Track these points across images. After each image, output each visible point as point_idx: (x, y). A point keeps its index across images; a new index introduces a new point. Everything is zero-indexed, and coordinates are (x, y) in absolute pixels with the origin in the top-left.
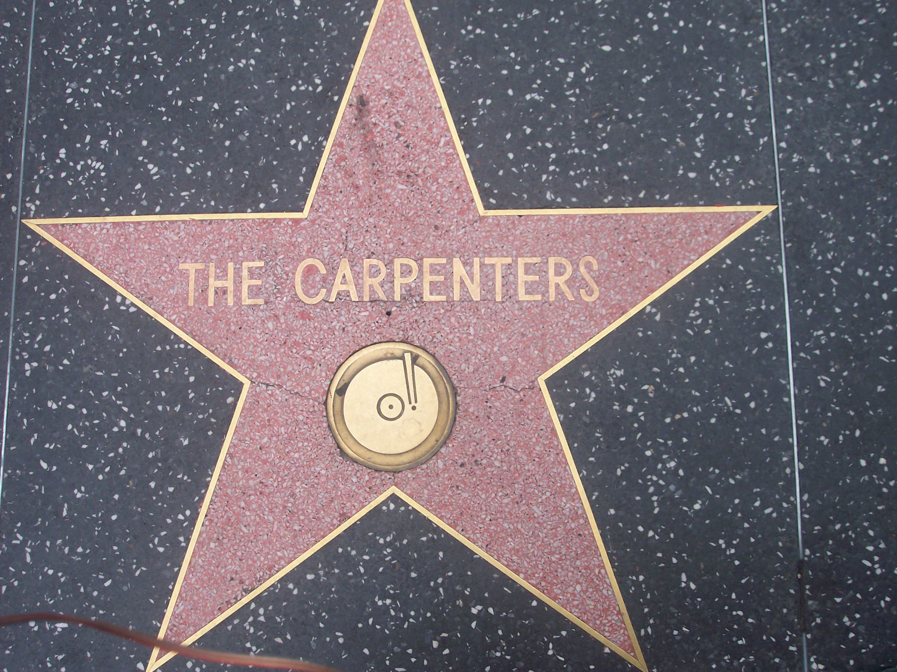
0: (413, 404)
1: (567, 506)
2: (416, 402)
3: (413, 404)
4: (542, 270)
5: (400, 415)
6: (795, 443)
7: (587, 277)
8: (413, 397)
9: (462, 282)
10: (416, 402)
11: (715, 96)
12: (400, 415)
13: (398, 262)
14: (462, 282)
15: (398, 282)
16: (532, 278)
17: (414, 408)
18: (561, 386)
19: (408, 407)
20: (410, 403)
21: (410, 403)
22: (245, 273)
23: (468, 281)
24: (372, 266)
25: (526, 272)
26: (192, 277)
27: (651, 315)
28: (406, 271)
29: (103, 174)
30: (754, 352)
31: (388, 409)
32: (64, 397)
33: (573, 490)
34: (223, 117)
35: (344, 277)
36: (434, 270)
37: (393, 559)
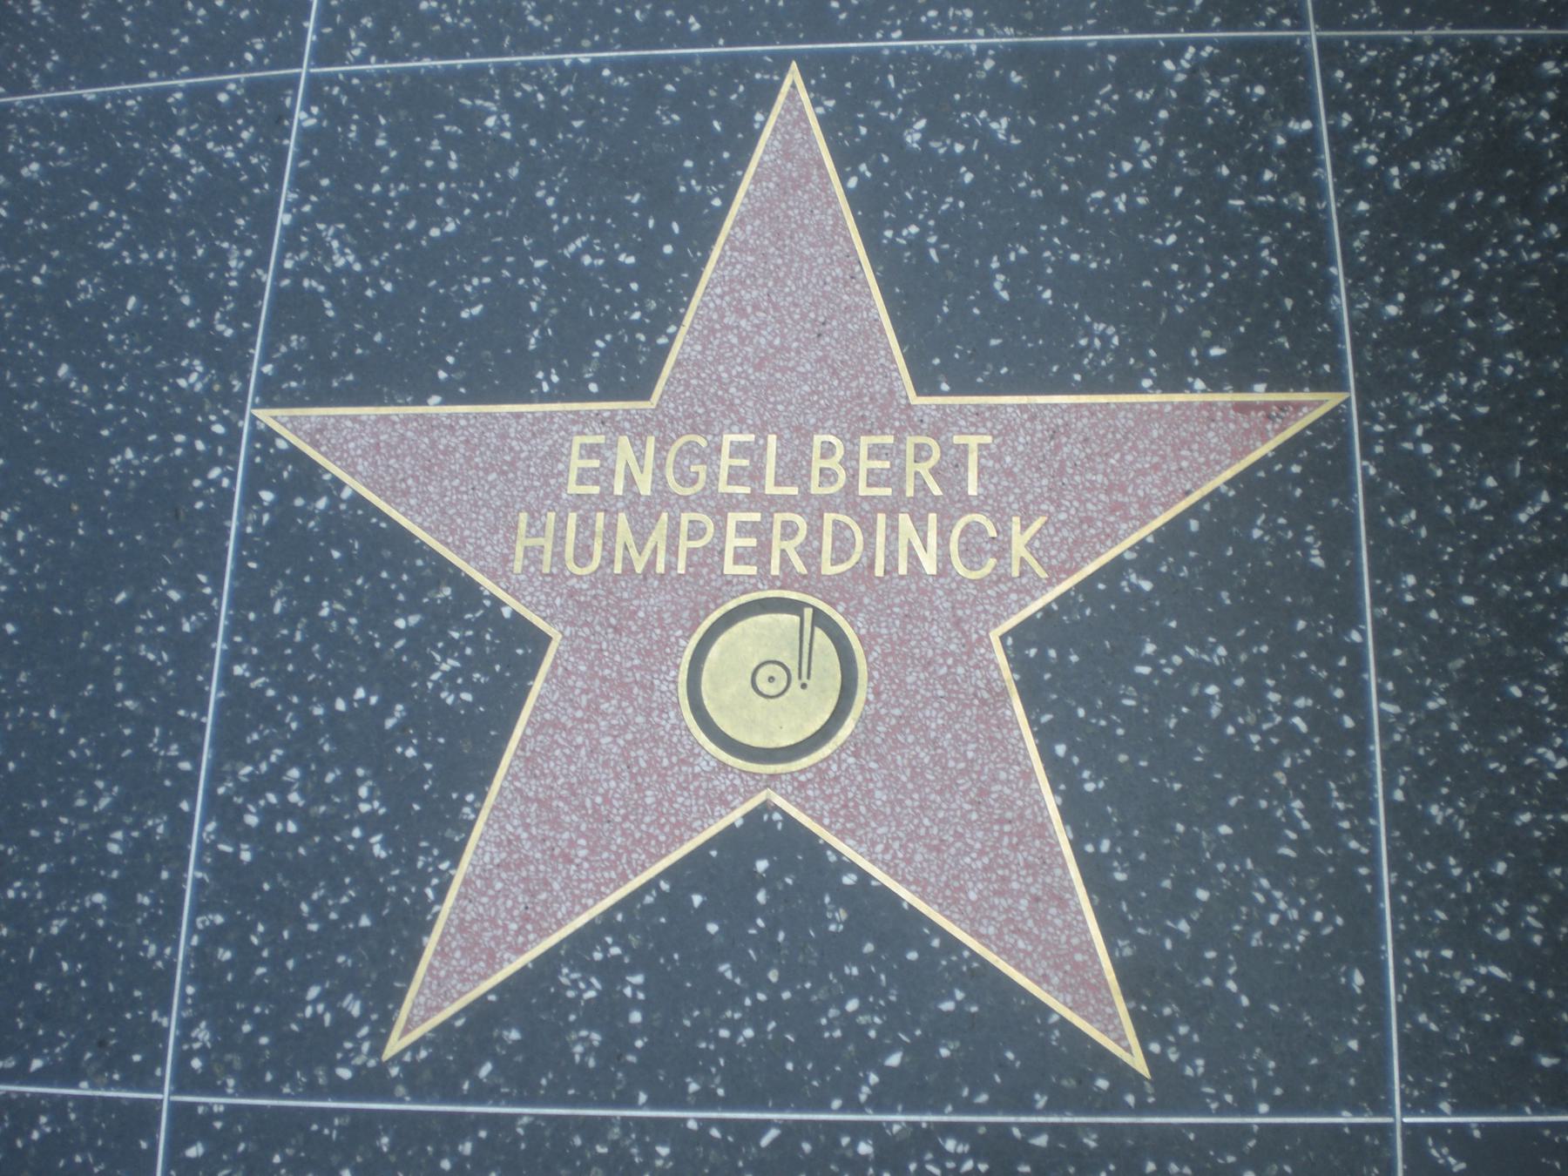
0: (804, 679)
1: (639, 856)
2: (809, 677)
3: (804, 679)
5: (785, 690)
6: (945, 1119)
8: (805, 653)
9: (911, 548)
10: (809, 677)
11: (1483, 404)
12: (785, 690)
14: (911, 548)
15: (684, 545)
16: (877, 464)
17: (804, 686)
19: (795, 683)
23: (917, 543)
24: (785, 524)
27: (281, 139)
28: (828, 451)
29: (450, 359)
30: (442, 116)
31: (765, 691)
33: (697, 824)
36: (875, 452)
37: (1522, 427)
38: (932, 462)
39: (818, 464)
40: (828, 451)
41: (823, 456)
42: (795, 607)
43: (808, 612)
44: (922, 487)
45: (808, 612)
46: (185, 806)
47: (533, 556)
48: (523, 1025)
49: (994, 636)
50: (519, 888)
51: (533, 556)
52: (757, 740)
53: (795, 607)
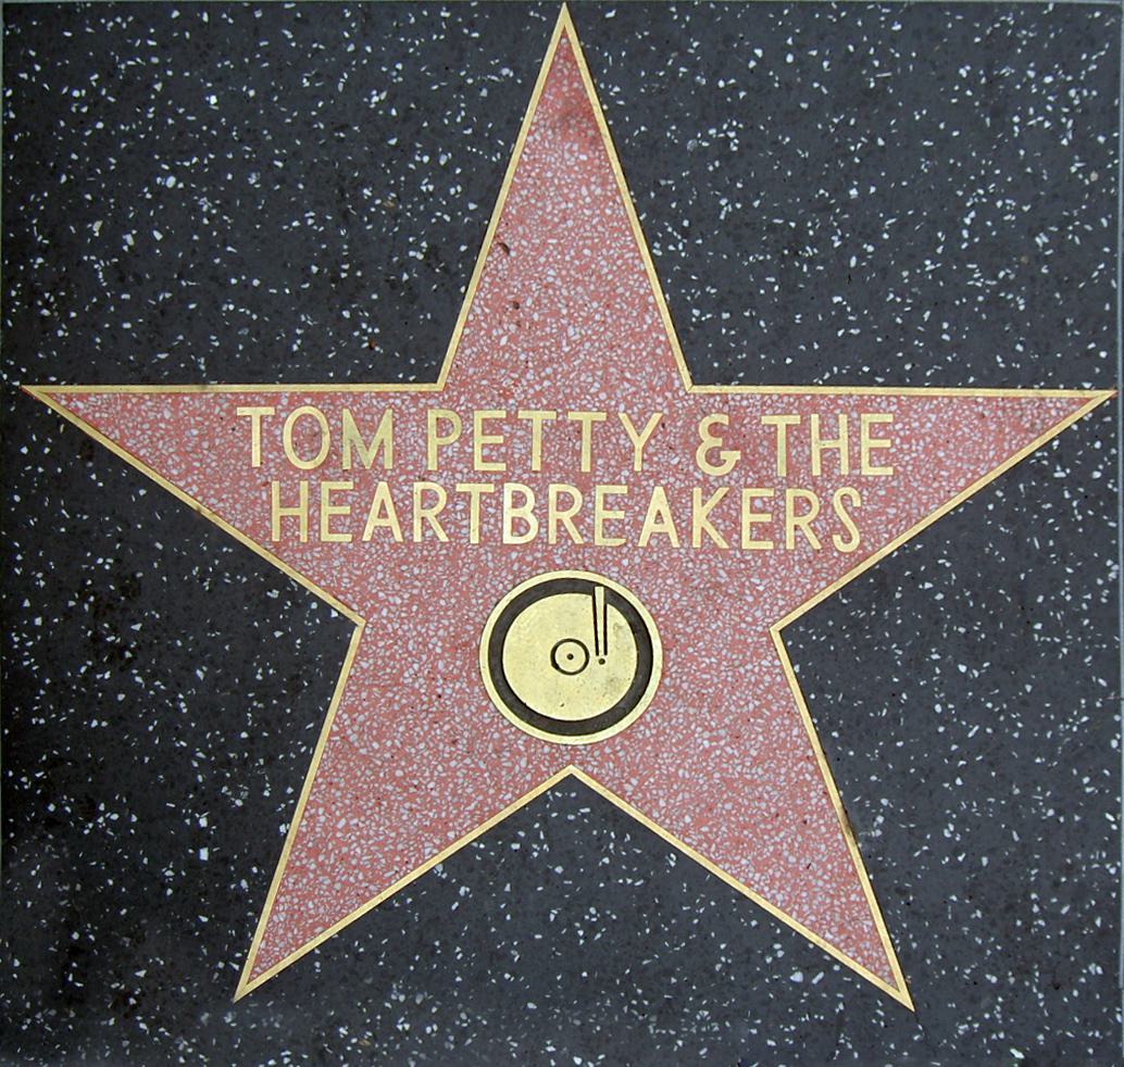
2: (606, 653)
4: (776, 508)
7: (845, 518)
8: (601, 645)
10: (606, 653)
13: (553, 489)
18: (804, 638)
20: (597, 654)
21: (597, 654)
22: (325, 495)
25: (753, 510)
26: (782, 434)
28: (519, 500)
31: (562, 662)
32: (289, 120)
34: (268, 1027)
35: (659, 514)
38: (440, 507)
39: (509, 513)
40: (519, 500)
41: (515, 506)
42: (587, 588)
43: (599, 592)
44: (800, 539)
45: (599, 592)
46: (334, 614)
47: (830, 458)
48: (400, 941)
49: (439, 386)
50: (347, 851)
51: (830, 458)
52: (578, 668)
53: (587, 588)
